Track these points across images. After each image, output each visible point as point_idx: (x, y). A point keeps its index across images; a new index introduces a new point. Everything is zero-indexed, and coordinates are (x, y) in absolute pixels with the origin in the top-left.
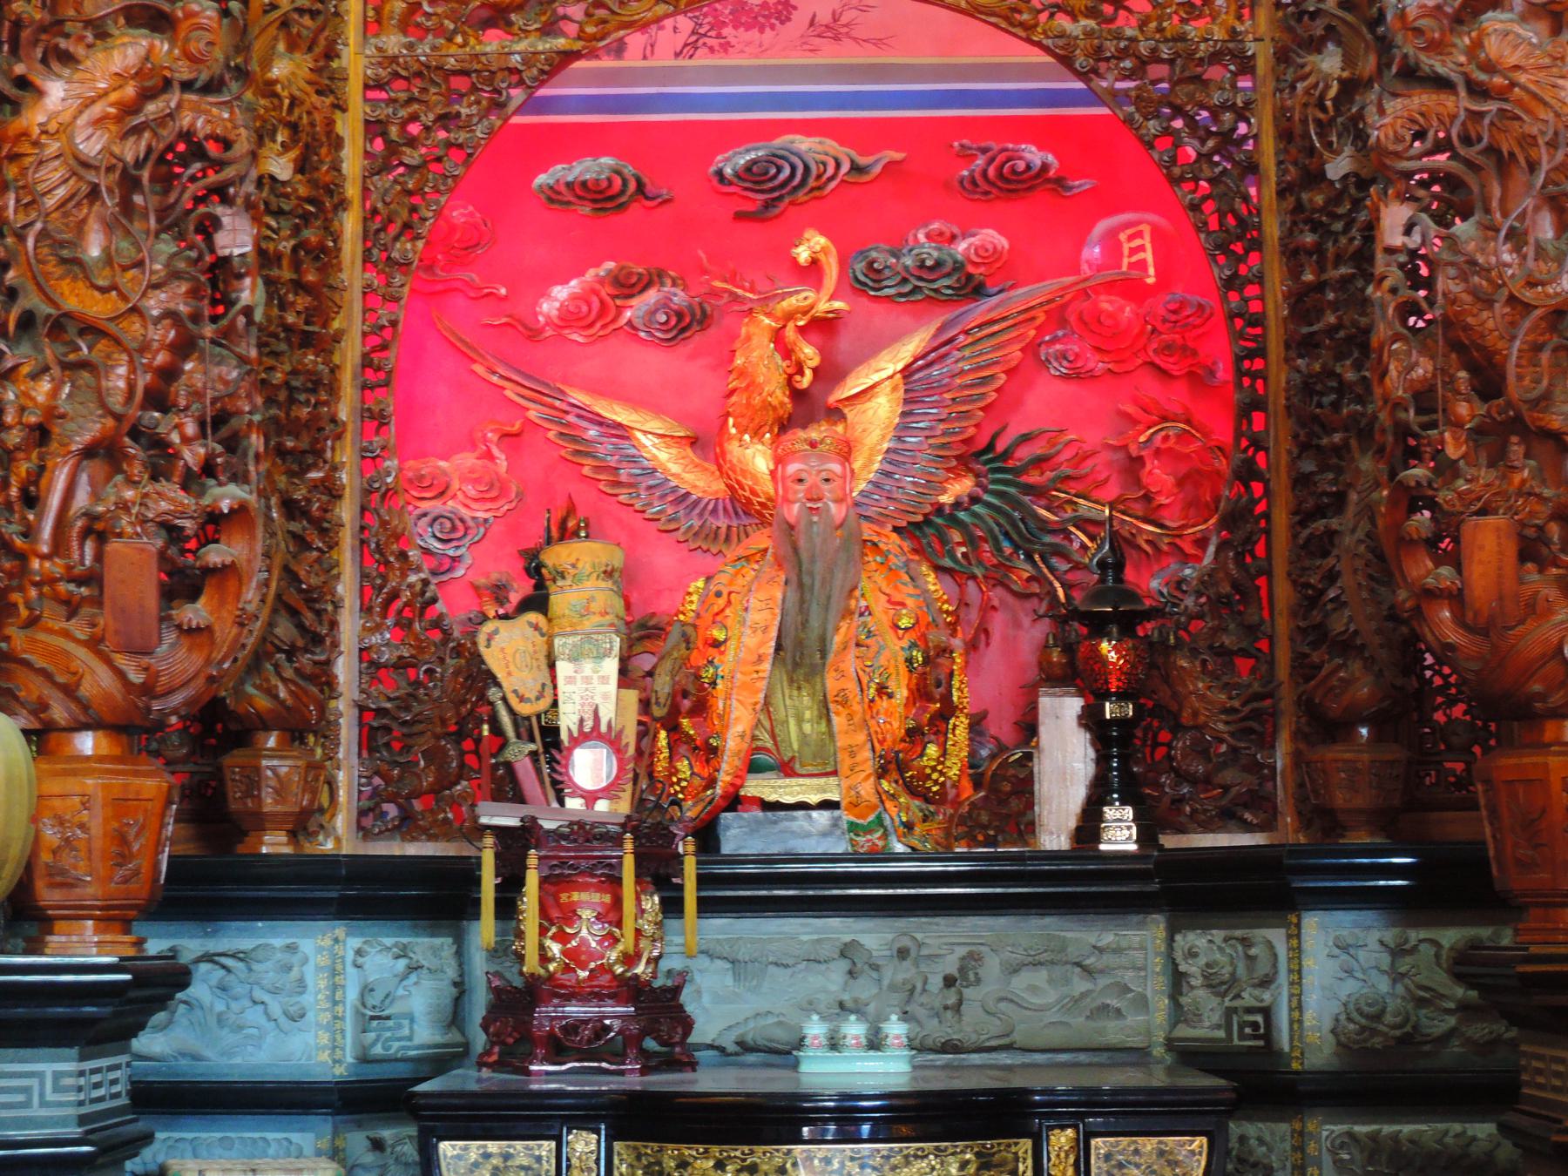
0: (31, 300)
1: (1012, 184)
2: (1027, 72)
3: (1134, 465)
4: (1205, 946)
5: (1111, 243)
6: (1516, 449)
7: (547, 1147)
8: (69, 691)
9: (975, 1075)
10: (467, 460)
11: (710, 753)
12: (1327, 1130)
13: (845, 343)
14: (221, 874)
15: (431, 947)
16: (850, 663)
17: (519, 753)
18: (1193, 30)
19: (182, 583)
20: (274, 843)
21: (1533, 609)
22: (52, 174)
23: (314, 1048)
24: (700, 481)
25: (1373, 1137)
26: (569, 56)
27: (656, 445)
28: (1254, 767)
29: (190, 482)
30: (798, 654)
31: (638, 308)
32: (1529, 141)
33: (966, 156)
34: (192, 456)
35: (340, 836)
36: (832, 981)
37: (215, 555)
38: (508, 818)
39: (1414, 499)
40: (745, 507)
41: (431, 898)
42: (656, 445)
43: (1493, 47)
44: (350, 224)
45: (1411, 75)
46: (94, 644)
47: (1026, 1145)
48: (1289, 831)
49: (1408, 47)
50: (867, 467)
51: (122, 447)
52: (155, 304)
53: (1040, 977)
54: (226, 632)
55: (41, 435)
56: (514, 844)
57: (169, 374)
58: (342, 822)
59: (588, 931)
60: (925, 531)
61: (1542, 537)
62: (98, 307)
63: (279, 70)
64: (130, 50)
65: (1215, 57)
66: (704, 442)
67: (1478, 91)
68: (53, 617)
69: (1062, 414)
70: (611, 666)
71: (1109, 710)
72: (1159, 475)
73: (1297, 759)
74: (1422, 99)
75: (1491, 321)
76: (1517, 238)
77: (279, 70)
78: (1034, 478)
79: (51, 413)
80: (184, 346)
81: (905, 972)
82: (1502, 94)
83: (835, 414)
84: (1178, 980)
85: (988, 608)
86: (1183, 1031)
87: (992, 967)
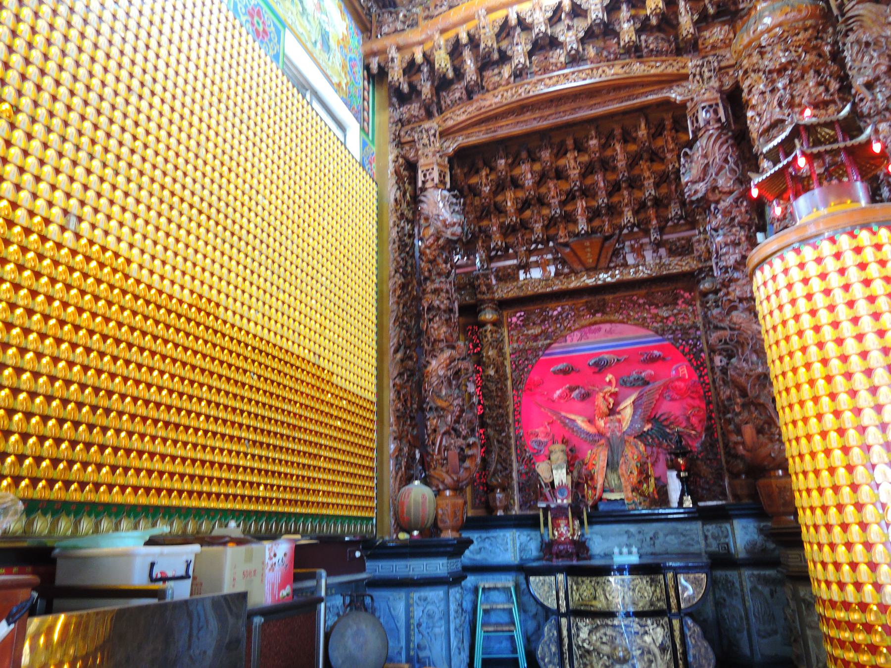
0: (432, 404)
1: (652, 360)
2: (646, 336)
3: (688, 419)
4: (711, 528)
5: (677, 370)
6: (753, 408)
7: (553, 578)
8: (443, 482)
9: (647, 560)
10: (542, 429)
11: (595, 489)
12: (746, 573)
13: (620, 397)
14: (488, 520)
15: (533, 534)
16: (624, 467)
17: (546, 491)
18: (685, 323)
19: (463, 458)
20: (500, 513)
21: (763, 445)
22: (434, 379)
23: (510, 557)
24: (591, 429)
25: (759, 575)
26: (550, 345)
27: (581, 422)
28: (720, 486)
29: (465, 438)
30: (612, 465)
31: (575, 394)
32: (746, 339)
33: (642, 355)
34: (464, 433)
35: (516, 510)
36: (624, 539)
37: (470, 452)
38: (543, 505)
39: (729, 421)
40: (601, 434)
41: (530, 523)
42: (581, 422)
43: (735, 319)
44: (509, 383)
45: (716, 328)
46: (447, 472)
47: (661, 577)
48: (730, 499)
49: (715, 322)
50: (625, 426)
51: (452, 431)
52: (455, 403)
53: (673, 537)
54: (473, 468)
55: (435, 431)
56: (546, 510)
57: (459, 417)
58: (516, 507)
59: (563, 529)
60: (641, 436)
61: (762, 427)
62: (444, 404)
63: (490, 353)
64: (447, 353)
65: (690, 328)
66: (591, 421)
67: (731, 329)
68: (439, 467)
69: (670, 408)
70: (564, 471)
71: (682, 474)
72: (694, 420)
73: (729, 484)
74: (720, 333)
75: (742, 380)
76: (746, 360)
77: (490, 353)
78: (665, 423)
79: (436, 426)
80: (462, 411)
81: (641, 537)
82: (739, 329)
83: (619, 413)
84: (706, 537)
85: (658, 453)
86: (709, 549)
87: (661, 535)
